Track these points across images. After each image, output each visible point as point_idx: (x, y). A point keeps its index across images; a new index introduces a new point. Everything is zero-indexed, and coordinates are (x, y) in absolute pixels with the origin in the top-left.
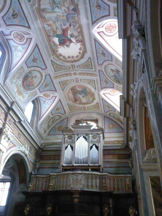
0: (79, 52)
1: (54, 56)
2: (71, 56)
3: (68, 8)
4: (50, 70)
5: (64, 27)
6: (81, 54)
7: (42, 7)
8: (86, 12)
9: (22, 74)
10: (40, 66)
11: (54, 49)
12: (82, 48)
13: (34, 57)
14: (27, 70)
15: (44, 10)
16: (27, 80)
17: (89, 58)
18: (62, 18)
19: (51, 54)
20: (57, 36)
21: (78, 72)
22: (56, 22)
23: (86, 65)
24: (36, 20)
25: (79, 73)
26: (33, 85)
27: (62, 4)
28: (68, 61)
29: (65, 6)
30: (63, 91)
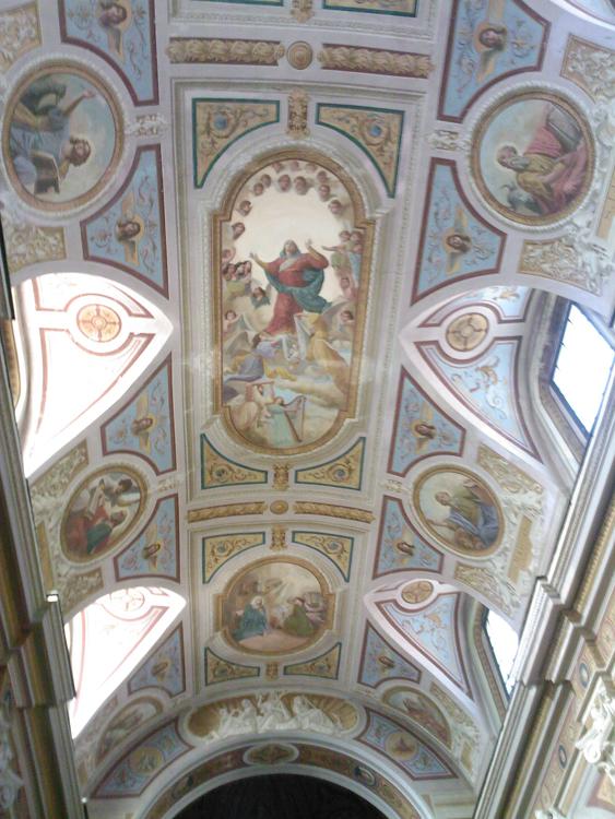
0: (247, 213)
1: (368, 216)
2: (292, 193)
3: (249, 398)
4: (423, 136)
5: (282, 336)
6: (237, 205)
7: (335, 413)
8: (187, 392)
9: (545, 243)
10: (454, 193)
11: (356, 249)
12: (228, 234)
13: (453, 256)
14: (518, 233)
15: (331, 404)
16: (547, 186)
17: (201, 186)
18: (280, 369)
19: (377, 228)
20: (320, 305)
21: (268, 516)
22: (307, 358)
23: (224, 124)
24: (369, 386)
25: (275, 63)
26: (548, 125)
27: (265, 409)
28: (315, 160)
29: (259, 404)
30: (364, 435)
